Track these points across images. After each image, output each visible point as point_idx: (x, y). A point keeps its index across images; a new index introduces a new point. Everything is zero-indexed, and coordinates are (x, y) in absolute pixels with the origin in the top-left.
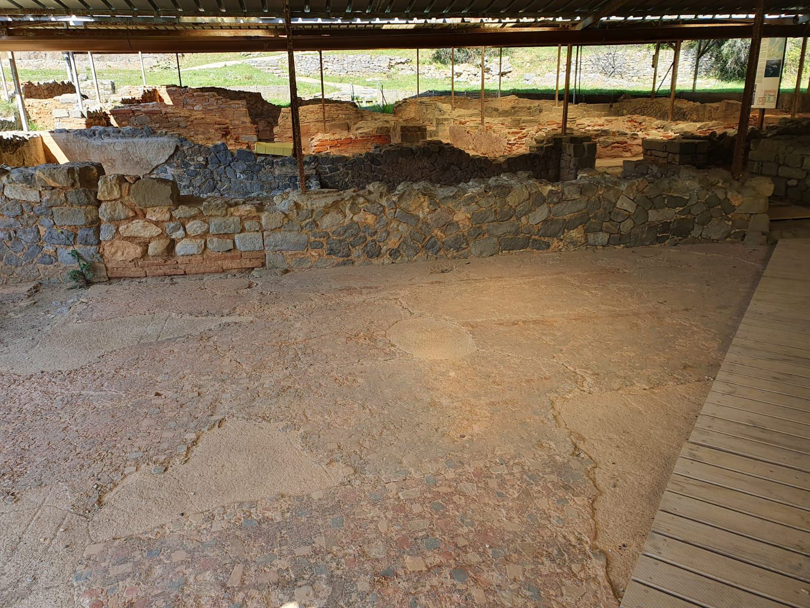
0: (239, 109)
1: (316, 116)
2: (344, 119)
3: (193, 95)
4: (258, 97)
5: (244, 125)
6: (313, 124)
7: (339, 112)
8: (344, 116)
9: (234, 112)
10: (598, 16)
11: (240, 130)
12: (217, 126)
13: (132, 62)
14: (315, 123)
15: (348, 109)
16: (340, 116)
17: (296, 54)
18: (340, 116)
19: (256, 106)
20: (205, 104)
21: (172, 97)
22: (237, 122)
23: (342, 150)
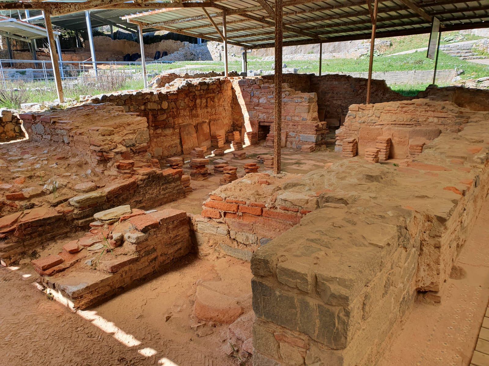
0: (301, 104)
1: (394, 118)
2: (436, 124)
3: (260, 87)
4: (380, 84)
5: (304, 122)
6: (387, 127)
7: (430, 113)
8: (436, 120)
9: (296, 106)
10: (134, 349)
11: (299, 127)
12: (92, 148)
13: (350, 53)
14: (391, 126)
15: (445, 110)
16: (431, 119)
17: (323, 44)
18: (431, 119)
19: (377, 95)
20: (269, 97)
21: (242, 89)
22: (297, 119)
23: (245, 225)
